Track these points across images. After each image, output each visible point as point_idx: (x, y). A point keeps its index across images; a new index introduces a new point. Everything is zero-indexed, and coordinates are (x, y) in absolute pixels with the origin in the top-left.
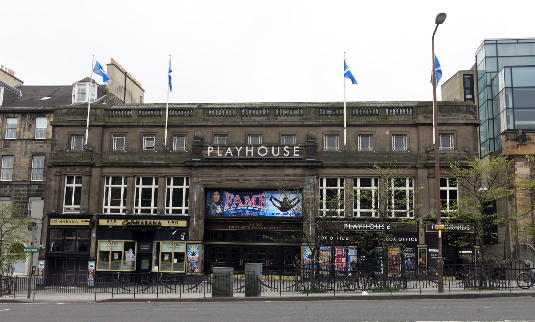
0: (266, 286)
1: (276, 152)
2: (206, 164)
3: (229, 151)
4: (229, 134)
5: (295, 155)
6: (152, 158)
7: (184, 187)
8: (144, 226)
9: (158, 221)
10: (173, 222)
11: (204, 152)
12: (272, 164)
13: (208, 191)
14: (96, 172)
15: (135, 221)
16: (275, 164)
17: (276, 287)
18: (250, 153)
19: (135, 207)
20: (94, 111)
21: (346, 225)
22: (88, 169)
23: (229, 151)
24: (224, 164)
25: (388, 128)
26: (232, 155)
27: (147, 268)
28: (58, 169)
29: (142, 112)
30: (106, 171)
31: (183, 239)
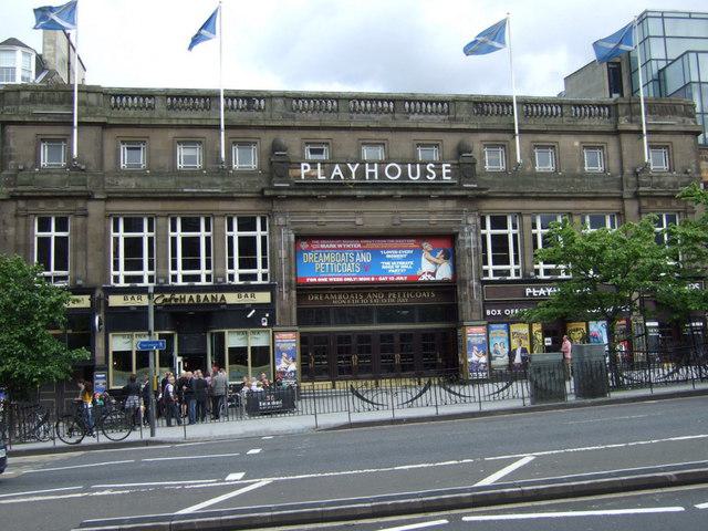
0: (367, 401)
1: (414, 174)
2: (301, 193)
3: (337, 171)
5: (444, 177)
6: (199, 182)
7: (258, 233)
8: (194, 305)
9: (219, 295)
10: (246, 296)
12: (411, 193)
14: (95, 209)
15: (177, 296)
16: (415, 193)
18: (372, 174)
19: (171, 272)
20: (84, 95)
21: (528, 291)
22: (81, 204)
23: (337, 171)
24: (331, 193)
28: (22, 204)
29: (172, 99)
30: (115, 206)
31: (265, 324)
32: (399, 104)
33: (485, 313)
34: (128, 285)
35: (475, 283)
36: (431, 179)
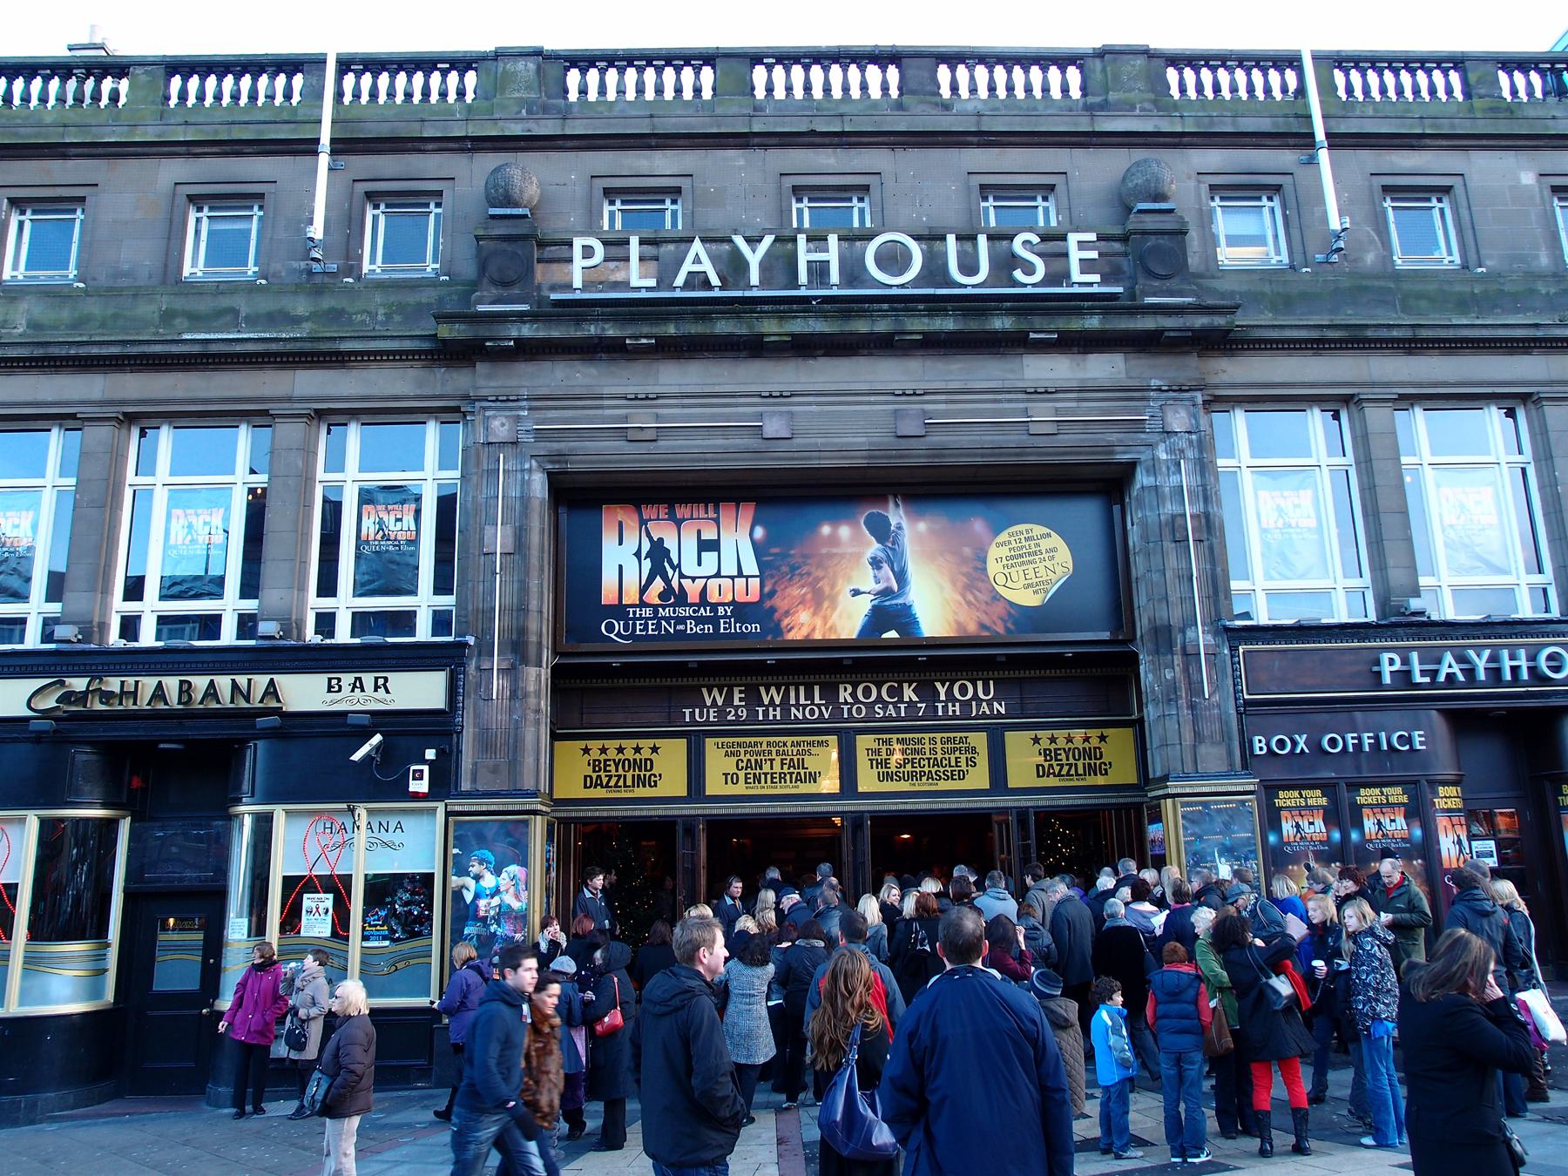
4: (684, 183)
5: (1076, 276)
8: (171, 715)
9: (261, 681)
10: (358, 685)
13: (581, 497)
15: (113, 684)
18: (819, 272)
23: (699, 259)
24: (671, 330)
25: (1524, 156)
27: (193, 984)
31: (421, 786)
32: (916, 70)
33: (1246, 746)
34: (357, 641)
35: (1202, 638)
36: (1031, 280)
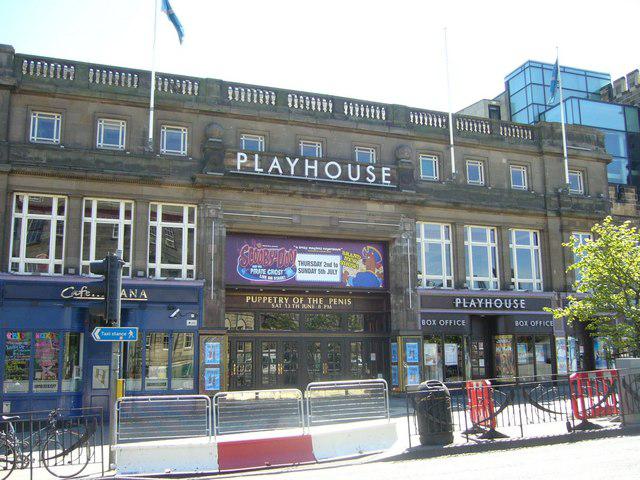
5: (384, 181)
11: (228, 162)
17: (564, 411)
23: (276, 164)
26: (281, 171)
